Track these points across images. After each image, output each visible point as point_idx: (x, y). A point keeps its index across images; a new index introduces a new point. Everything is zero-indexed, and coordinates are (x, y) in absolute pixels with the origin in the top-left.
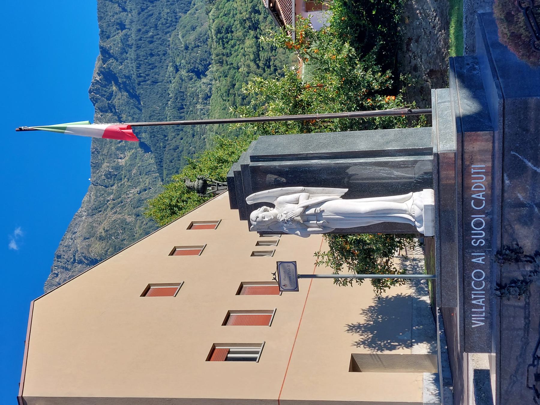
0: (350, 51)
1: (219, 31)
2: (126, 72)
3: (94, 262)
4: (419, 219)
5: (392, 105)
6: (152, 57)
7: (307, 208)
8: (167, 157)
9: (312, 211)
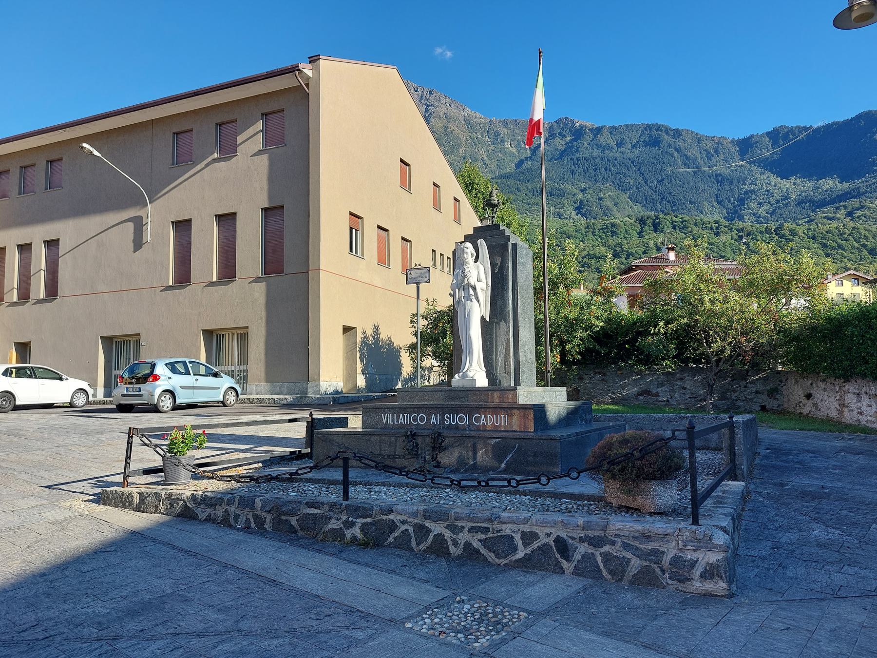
0: (597, 326)
1: (613, 225)
2: (582, 148)
3: (427, 120)
4: (465, 376)
5: (553, 359)
6: (594, 171)
7: (474, 289)
8: (512, 182)
9: (472, 292)
